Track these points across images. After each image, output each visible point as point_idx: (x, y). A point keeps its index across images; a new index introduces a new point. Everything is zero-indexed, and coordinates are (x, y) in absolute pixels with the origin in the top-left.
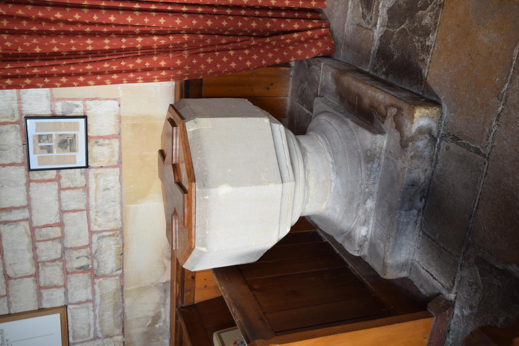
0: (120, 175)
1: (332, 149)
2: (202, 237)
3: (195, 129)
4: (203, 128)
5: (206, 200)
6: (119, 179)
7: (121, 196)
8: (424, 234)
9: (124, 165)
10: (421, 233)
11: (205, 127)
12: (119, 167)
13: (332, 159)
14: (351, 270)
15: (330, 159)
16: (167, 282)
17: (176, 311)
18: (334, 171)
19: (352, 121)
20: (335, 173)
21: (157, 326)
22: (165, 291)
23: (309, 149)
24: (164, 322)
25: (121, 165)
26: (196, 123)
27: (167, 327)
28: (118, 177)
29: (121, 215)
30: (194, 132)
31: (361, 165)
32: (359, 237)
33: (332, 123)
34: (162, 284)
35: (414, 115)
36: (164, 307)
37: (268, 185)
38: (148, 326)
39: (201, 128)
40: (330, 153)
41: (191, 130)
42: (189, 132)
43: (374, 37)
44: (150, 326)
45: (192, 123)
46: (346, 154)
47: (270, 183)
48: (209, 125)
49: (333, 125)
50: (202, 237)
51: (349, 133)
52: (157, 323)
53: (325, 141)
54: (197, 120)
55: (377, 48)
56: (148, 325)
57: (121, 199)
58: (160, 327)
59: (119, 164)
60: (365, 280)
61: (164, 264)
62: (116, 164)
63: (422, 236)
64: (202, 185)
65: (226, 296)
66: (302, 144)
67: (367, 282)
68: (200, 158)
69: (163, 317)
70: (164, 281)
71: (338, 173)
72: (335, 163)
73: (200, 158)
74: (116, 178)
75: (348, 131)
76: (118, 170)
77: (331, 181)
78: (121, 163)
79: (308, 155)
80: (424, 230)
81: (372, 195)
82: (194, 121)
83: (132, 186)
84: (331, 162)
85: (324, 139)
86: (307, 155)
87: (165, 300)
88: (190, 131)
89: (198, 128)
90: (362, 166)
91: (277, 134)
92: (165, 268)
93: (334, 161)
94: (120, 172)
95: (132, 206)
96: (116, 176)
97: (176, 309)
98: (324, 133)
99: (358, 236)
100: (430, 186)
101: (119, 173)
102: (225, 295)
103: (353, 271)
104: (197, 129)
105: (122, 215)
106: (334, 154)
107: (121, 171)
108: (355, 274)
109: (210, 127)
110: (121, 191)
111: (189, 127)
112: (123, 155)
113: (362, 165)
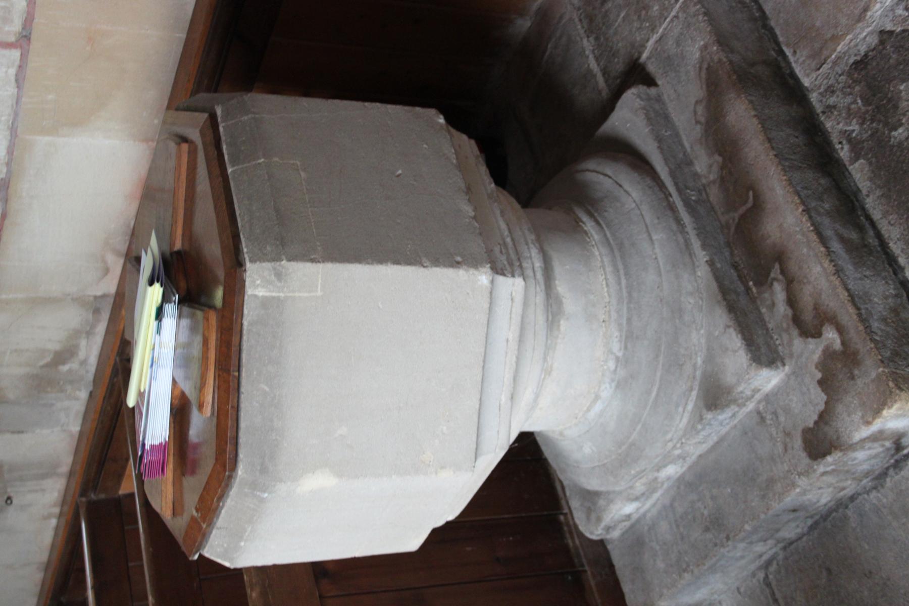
0: (20, 67)
1: (629, 320)
2: (225, 545)
3: (274, 294)
4: (297, 294)
5: (262, 500)
6: (16, 75)
7: (16, 114)
8: (767, 582)
9: (35, 45)
10: (761, 575)
11: (301, 294)
12: (21, 47)
13: (620, 349)
14: (565, 528)
15: (616, 347)
16: (104, 296)
17: (115, 360)
18: (613, 380)
19: (711, 263)
20: (613, 385)
21: (65, 368)
22: (97, 311)
23: (570, 303)
24: (84, 363)
25: (29, 45)
26: (279, 275)
27: (87, 372)
28: (12, 71)
29: (8, 152)
30: (265, 303)
31: (687, 400)
32: (612, 518)
33: (655, 237)
34: (92, 299)
35: (883, 409)
36: (88, 338)
37: (436, 473)
38: (42, 367)
39: (291, 294)
40: (620, 330)
41: (261, 292)
42: (252, 295)
43: (869, 14)
44: (46, 366)
45: (266, 273)
46: (661, 358)
47: (442, 468)
48: (317, 287)
49: (656, 246)
50: (225, 545)
51: (692, 301)
52: (64, 363)
53: (620, 284)
54: (283, 267)
55: (863, 49)
56: (42, 363)
57: (15, 120)
58: (70, 371)
59: (24, 39)
60: (589, 573)
61: (104, 261)
62: (12, 39)
63: (759, 581)
64: (259, 468)
65: (254, 595)
66: (557, 282)
67: (593, 583)
68: (267, 389)
69: (82, 354)
70: (99, 293)
71: (621, 385)
72: (624, 361)
73: (267, 389)
74: (6, 72)
75: (691, 294)
76: (16, 54)
77: (597, 397)
78: (29, 39)
79: (562, 328)
80: (771, 577)
81: (684, 459)
82: (275, 269)
83: (50, 97)
84: (615, 354)
85: (619, 279)
86: (559, 326)
87: (93, 326)
88: (256, 296)
89: (282, 295)
90: (689, 402)
91: (503, 307)
92: (107, 271)
93: (624, 354)
94: (21, 59)
95: (43, 140)
96: (8, 67)
97: (118, 359)
98: (623, 257)
99: (612, 515)
100: (834, 514)
101: (17, 63)
102: (252, 590)
103: (568, 536)
104: (278, 298)
105: (12, 154)
106: (630, 337)
107: (24, 57)
108: (571, 544)
109: (319, 293)
110: (17, 103)
111: (254, 282)
112: (36, 21)
113: (690, 399)
